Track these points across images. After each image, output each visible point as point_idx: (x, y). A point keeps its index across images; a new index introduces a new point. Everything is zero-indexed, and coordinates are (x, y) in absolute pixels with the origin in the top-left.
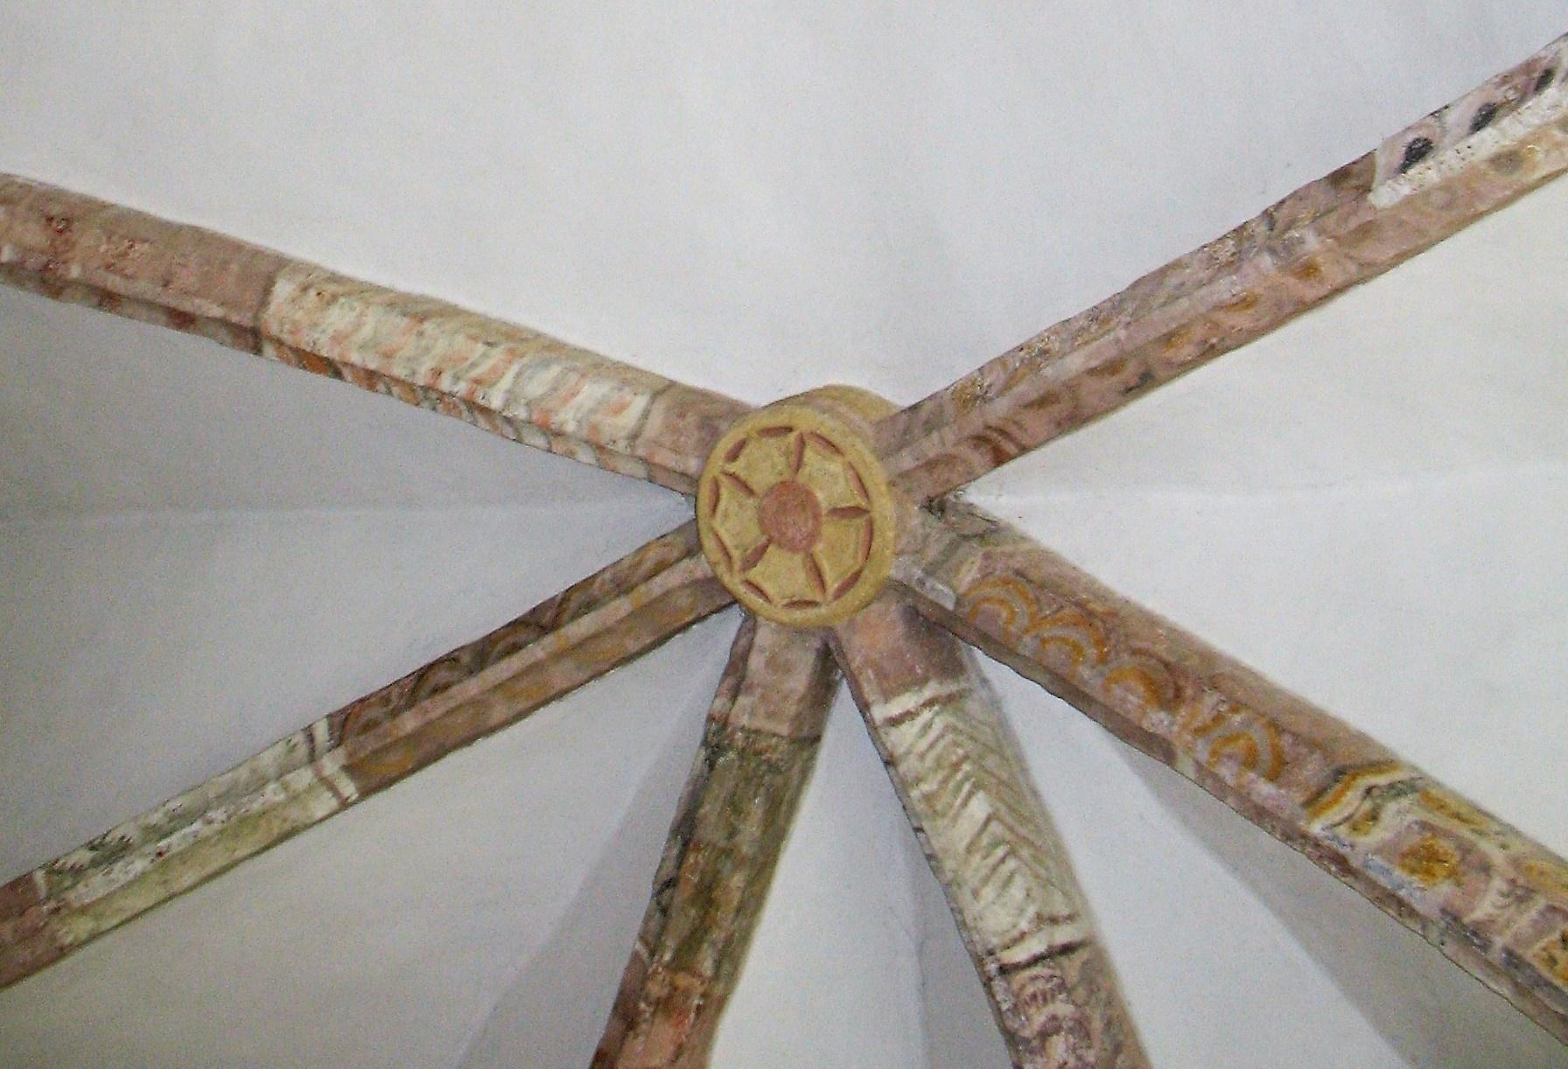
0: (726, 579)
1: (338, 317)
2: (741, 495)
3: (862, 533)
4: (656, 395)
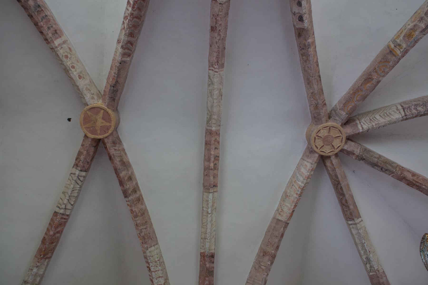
0: (336, 152)
1: (285, 209)
2: (323, 147)
3: (333, 128)
4: (304, 160)
